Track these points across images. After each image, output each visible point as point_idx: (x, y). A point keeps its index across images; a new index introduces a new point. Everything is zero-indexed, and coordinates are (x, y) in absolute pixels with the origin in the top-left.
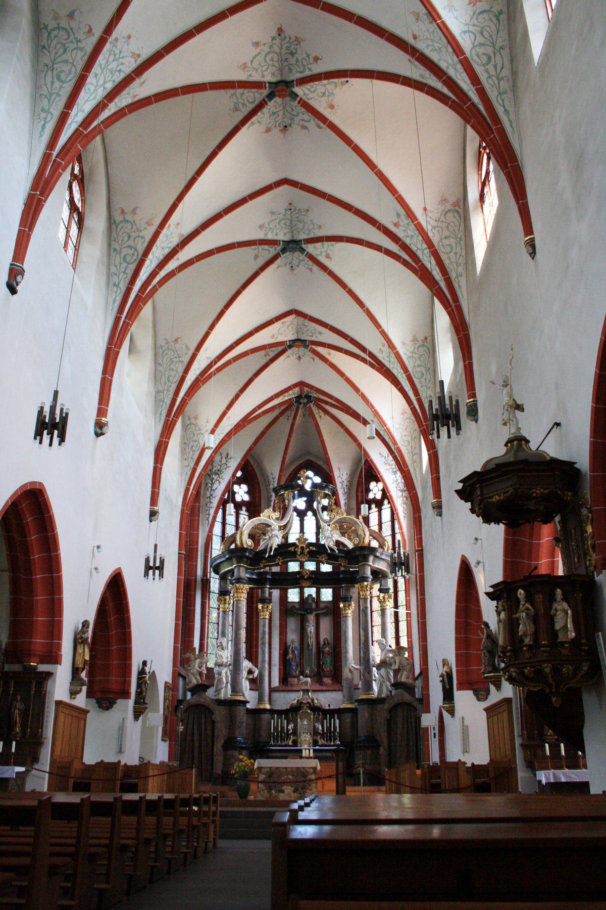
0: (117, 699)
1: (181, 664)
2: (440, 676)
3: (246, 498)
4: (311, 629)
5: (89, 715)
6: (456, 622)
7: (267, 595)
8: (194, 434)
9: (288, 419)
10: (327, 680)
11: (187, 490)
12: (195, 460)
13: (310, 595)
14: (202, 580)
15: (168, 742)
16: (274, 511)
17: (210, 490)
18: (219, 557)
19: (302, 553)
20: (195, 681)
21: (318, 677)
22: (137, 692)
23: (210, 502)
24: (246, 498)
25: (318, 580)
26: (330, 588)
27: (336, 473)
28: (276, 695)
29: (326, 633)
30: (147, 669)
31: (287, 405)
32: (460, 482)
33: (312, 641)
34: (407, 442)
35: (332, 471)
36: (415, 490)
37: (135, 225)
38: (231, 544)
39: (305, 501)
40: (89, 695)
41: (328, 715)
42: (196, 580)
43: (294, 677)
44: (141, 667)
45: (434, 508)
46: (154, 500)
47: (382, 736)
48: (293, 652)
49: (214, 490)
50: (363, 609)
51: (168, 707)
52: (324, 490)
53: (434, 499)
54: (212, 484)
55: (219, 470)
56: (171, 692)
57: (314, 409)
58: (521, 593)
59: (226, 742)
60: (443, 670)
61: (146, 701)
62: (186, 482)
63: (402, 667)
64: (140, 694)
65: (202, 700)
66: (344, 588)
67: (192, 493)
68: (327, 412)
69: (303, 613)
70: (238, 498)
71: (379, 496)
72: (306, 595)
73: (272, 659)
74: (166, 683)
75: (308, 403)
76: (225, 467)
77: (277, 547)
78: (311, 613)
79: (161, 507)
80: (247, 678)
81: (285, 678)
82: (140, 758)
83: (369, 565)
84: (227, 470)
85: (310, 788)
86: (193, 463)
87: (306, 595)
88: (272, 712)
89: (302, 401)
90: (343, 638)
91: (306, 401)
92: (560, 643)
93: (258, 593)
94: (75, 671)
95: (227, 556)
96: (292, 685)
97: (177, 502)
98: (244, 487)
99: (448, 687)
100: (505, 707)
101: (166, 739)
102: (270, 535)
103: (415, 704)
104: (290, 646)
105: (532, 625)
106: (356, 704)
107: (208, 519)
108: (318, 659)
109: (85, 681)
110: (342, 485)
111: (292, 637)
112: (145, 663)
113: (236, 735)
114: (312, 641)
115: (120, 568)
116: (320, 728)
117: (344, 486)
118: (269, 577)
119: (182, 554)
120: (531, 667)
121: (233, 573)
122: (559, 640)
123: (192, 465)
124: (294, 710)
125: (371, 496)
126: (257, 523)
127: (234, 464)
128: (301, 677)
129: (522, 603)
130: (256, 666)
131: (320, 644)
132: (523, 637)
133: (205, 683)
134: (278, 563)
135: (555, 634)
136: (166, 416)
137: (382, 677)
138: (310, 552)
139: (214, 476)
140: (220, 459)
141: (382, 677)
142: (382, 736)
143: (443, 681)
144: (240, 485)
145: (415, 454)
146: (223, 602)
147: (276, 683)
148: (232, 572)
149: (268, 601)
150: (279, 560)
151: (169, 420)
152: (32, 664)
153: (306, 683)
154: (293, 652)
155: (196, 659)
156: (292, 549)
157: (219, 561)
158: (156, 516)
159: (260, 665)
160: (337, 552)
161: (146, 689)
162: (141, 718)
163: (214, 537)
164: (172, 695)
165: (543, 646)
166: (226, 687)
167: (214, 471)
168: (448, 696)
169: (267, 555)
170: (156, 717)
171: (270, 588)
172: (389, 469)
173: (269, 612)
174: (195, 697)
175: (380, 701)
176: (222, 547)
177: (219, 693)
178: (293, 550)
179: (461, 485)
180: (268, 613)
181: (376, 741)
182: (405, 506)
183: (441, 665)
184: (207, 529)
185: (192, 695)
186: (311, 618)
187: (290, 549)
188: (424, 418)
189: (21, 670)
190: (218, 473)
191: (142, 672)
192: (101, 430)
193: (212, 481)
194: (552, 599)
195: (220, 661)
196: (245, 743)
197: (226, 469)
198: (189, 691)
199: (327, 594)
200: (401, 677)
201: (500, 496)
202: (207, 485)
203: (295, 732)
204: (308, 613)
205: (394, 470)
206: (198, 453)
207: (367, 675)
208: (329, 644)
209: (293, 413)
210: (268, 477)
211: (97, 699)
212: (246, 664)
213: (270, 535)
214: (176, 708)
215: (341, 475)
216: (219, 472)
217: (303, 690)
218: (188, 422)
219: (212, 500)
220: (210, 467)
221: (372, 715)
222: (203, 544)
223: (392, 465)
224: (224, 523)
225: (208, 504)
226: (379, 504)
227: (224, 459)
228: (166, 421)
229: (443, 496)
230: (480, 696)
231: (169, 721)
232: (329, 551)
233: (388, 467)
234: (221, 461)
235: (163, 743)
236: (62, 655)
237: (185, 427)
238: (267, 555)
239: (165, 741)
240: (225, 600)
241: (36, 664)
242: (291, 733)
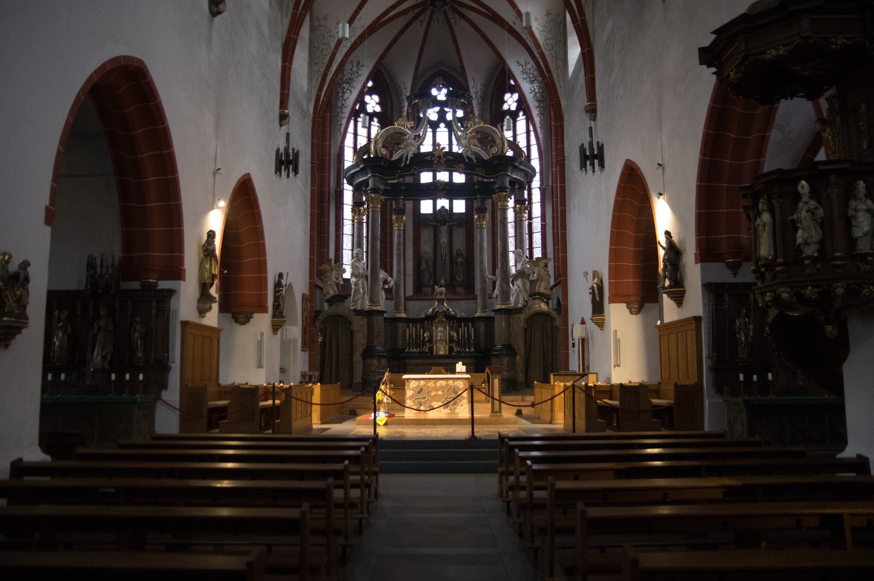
0: (254, 313)
1: (317, 276)
2: (590, 289)
3: (378, 109)
4: (444, 240)
5: (222, 334)
6: (612, 232)
7: (401, 206)
8: (324, 37)
9: (422, 24)
10: (460, 290)
11: (318, 97)
12: (326, 64)
13: (443, 207)
14: (336, 191)
15: (307, 353)
16: (409, 120)
17: (341, 100)
18: (350, 168)
19: (439, 162)
20: (332, 293)
21: (451, 286)
22: (274, 305)
23: (342, 112)
24: (378, 109)
25: (451, 191)
26: (462, 199)
27: (471, 84)
28: (411, 304)
29: (459, 243)
30: (284, 282)
31: (421, 8)
32: (713, 33)
33: (444, 251)
34: (550, 46)
35: (466, 81)
36: (558, 97)
37: (328, 27)
38: (364, 155)
39: (437, 112)
40: (224, 309)
41: (463, 324)
42: (329, 191)
43: (429, 286)
44: (277, 280)
45: (587, 111)
46: (284, 102)
47: (520, 345)
48: (427, 262)
49: (345, 100)
50: (501, 221)
51: (306, 318)
52: (460, 98)
53: (588, 102)
54: (344, 93)
55: (350, 79)
56: (308, 303)
57: (451, 14)
58: (804, 186)
59: (364, 351)
60: (592, 282)
61: (284, 314)
62: (317, 88)
63: (540, 278)
64: (277, 307)
65: (340, 311)
66: (479, 199)
67: (323, 99)
68: (463, 16)
69: (436, 224)
70: (370, 109)
71: (514, 107)
72: (438, 207)
73: (407, 269)
74: (303, 294)
75: (442, 6)
76: (356, 75)
77: (413, 156)
78: (444, 224)
79: (291, 110)
80: (383, 288)
81: (418, 288)
82: (281, 368)
83: (508, 176)
84: (359, 77)
85: (461, 404)
86: (324, 68)
87: (438, 207)
88: (408, 320)
89: (437, 3)
90: (496, 250)
91: (441, 4)
92: (860, 255)
93: (391, 204)
94: (204, 287)
95: (362, 166)
96: (426, 295)
97: (308, 108)
98: (376, 98)
99: (598, 299)
100: (694, 326)
101: (305, 349)
102: (406, 144)
103: (554, 314)
104: (423, 256)
105: (820, 231)
106: (494, 313)
107: (339, 130)
108: (452, 269)
109: (215, 298)
110: (476, 95)
111: (427, 248)
112: (281, 275)
113: (374, 344)
114: (444, 251)
115: (248, 174)
116: (455, 335)
117: (478, 97)
118: (403, 188)
119: (316, 163)
120: (813, 287)
121: (368, 183)
122: (859, 252)
123: (322, 70)
124: (431, 318)
125: (506, 107)
126: (392, 131)
127: (365, 72)
128: (436, 287)
129: (805, 198)
130: (391, 276)
131: (452, 256)
132: (802, 247)
133: (342, 293)
134: (414, 173)
135: (852, 242)
136: (294, 9)
137: (519, 287)
138: (448, 160)
139: (345, 85)
140: (351, 67)
141: (519, 287)
142: (520, 345)
143: (593, 293)
144: (371, 96)
145: (558, 59)
146: (357, 213)
147: (410, 292)
148: (366, 182)
149: (402, 212)
150: (415, 169)
151: (297, 13)
152: (151, 280)
153: (441, 293)
154: (427, 262)
155: (332, 270)
156: (429, 158)
157: (353, 171)
158: (287, 120)
159: (395, 275)
160: (475, 161)
161: (284, 302)
162: (279, 332)
163: (346, 149)
164: (310, 306)
165: (838, 258)
166: (363, 297)
167: (345, 80)
168: (598, 308)
169: (403, 165)
170: (294, 331)
171: (404, 200)
172: (526, 79)
173: (401, 225)
174: (332, 307)
175: (518, 311)
176: (355, 158)
177: (356, 305)
178: (429, 159)
179: (714, 36)
180: (402, 224)
181: (513, 349)
182: (542, 117)
183: (590, 276)
184: (340, 139)
185: (330, 306)
186: (444, 229)
187: (427, 158)
188: (579, 12)
189: (139, 287)
190: (350, 82)
191: (278, 285)
192: (217, 7)
193: (343, 90)
194: (850, 194)
195: (356, 272)
196: (383, 352)
197: (357, 77)
198: (327, 302)
199: (459, 206)
200: (539, 287)
201: (778, 51)
202: (338, 94)
203: (431, 340)
204: (442, 225)
205: (532, 79)
206: (328, 57)
207: (504, 285)
208: (462, 255)
209: (427, 18)
210: (400, 87)
211: (233, 314)
212: (382, 275)
213: (406, 144)
214: (315, 318)
215: (475, 87)
216: (350, 81)
217: (438, 300)
218: (317, 24)
219: (343, 111)
220: (340, 75)
221: (509, 324)
222: (336, 155)
223: (530, 73)
224: (356, 134)
225: (340, 114)
226: (514, 115)
227: (355, 66)
228: (294, 15)
229: (598, 99)
230: (633, 310)
231: (307, 331)
232: (467, 161)
233: (525, 76)
234: (351, 70)
235: (303, 353)
236: (185, 270)
237: (312, 29)
238: (403, 165)
239: (305, 351)
240: (360, 211)
241: (156, 281)
242: (427, 341)
